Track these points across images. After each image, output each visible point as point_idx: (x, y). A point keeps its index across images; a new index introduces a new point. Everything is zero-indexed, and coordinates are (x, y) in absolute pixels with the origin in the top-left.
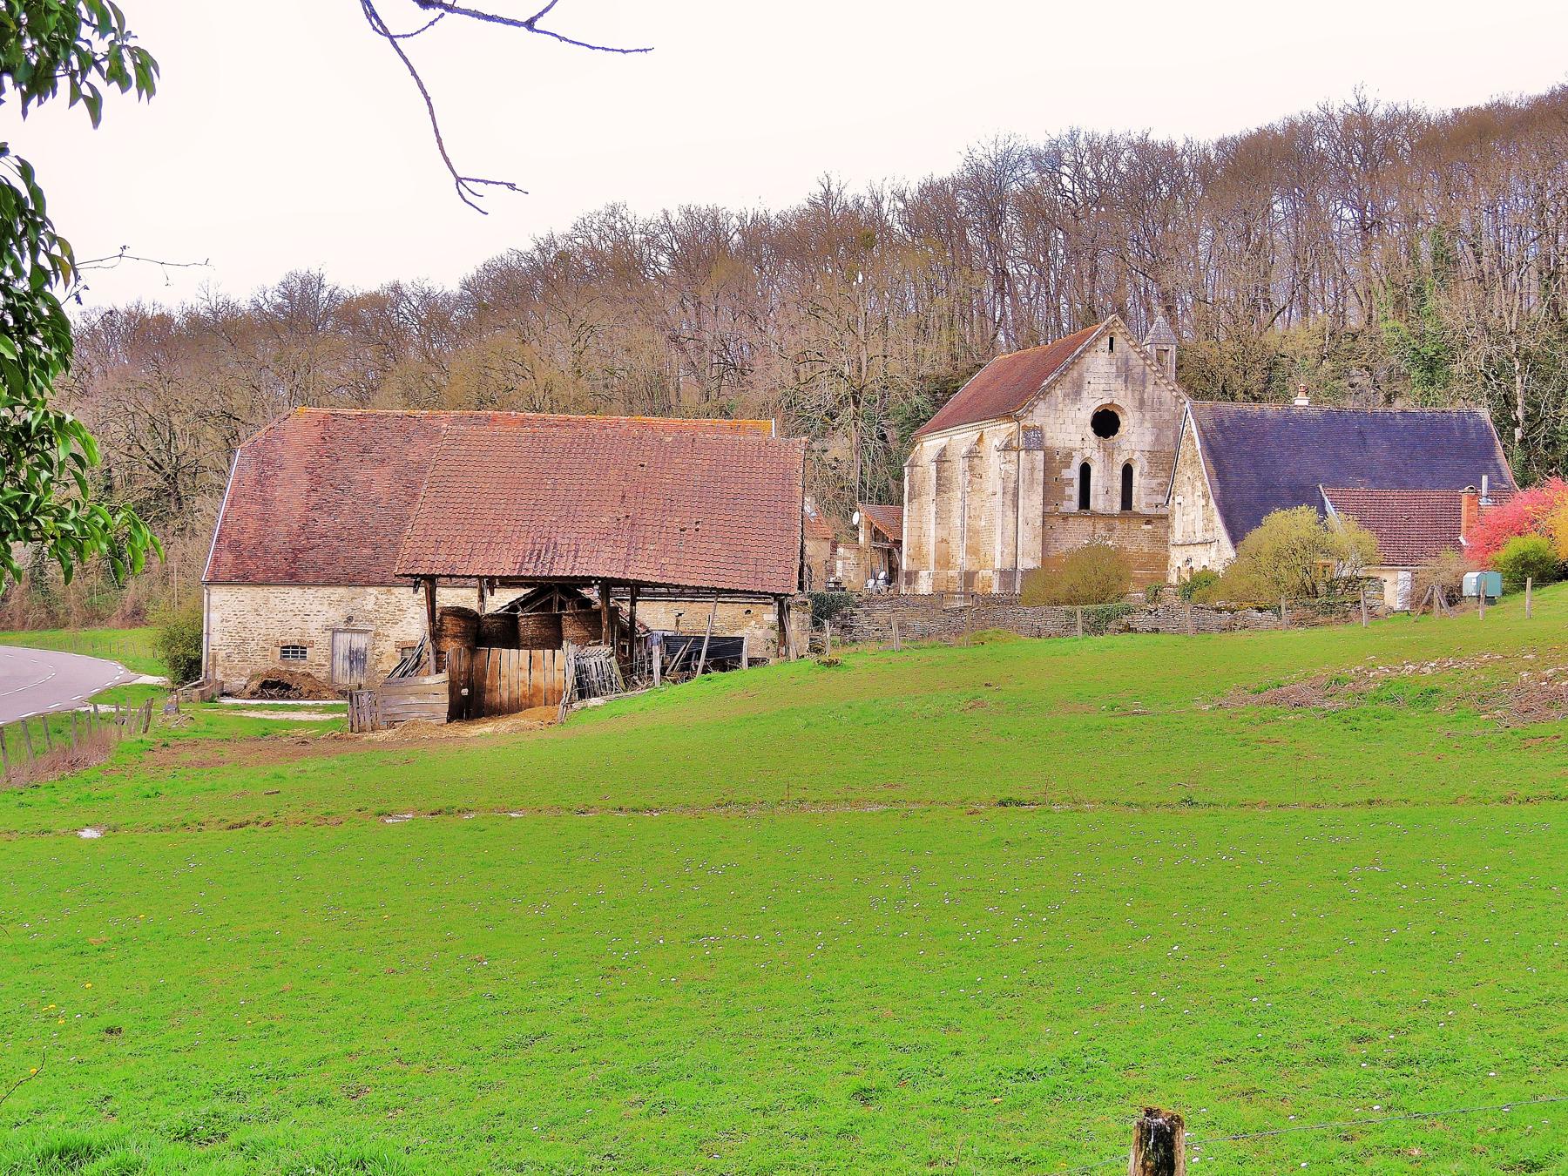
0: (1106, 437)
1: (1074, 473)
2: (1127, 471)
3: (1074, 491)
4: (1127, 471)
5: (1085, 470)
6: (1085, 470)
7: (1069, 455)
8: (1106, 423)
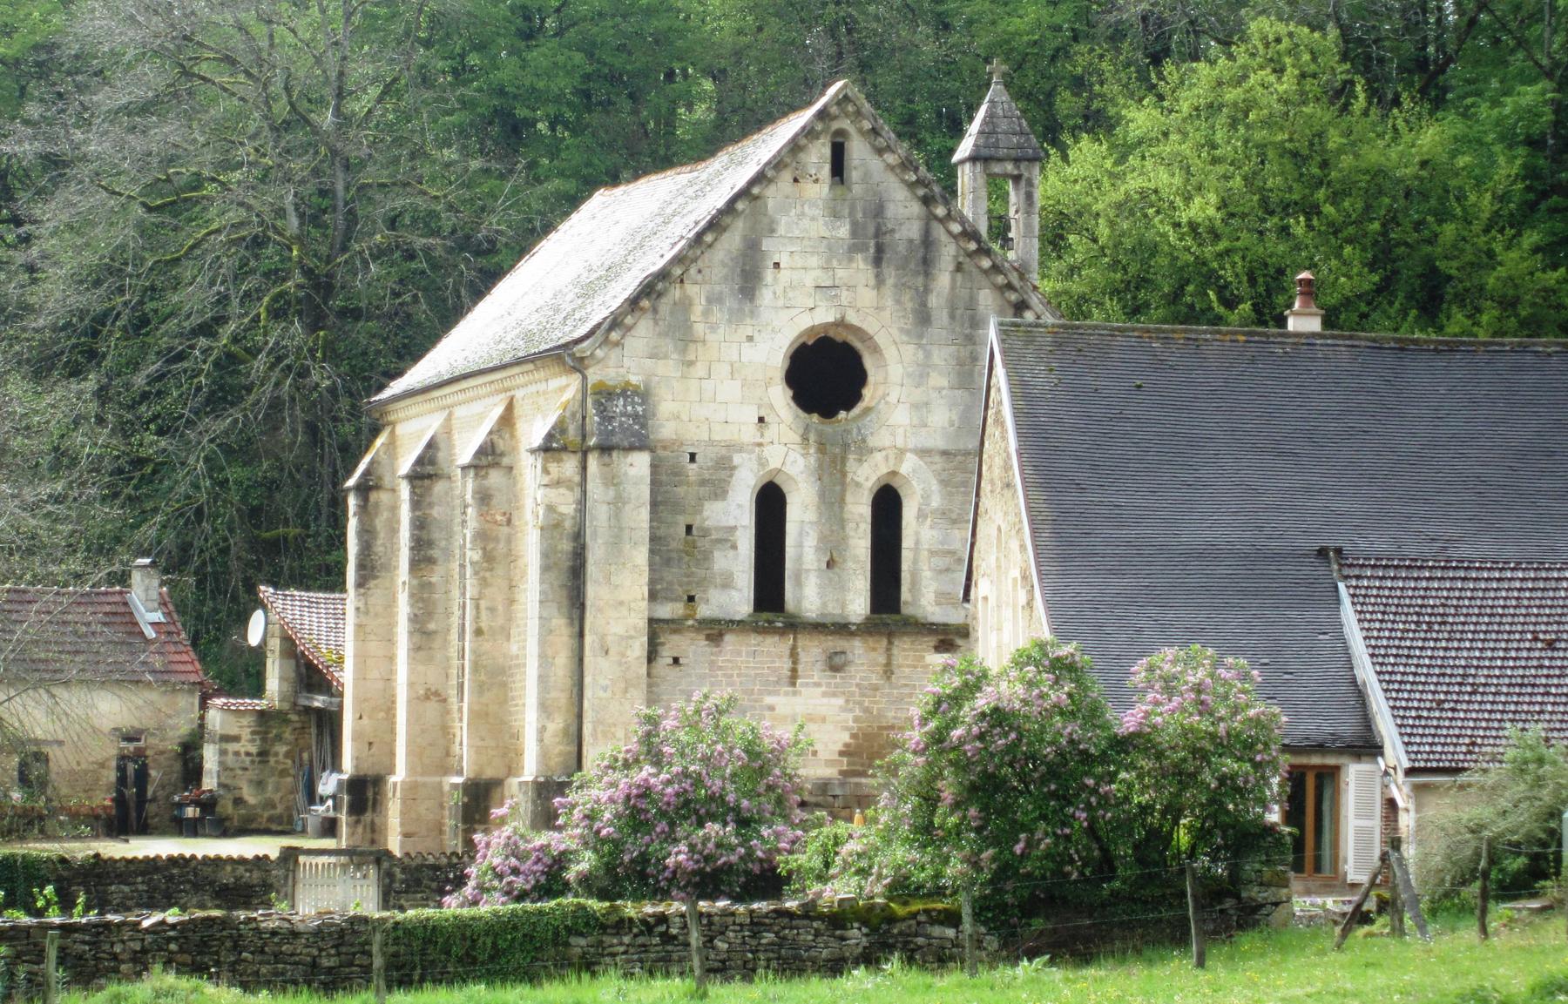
0: (828, 413)
1: (737, 512)
2: (887, 504)
3: (739, 562)
4: (887, 504)
5: (771, 502)
6: (771, 502)
7: (725, 466)
8: (826, 376)
